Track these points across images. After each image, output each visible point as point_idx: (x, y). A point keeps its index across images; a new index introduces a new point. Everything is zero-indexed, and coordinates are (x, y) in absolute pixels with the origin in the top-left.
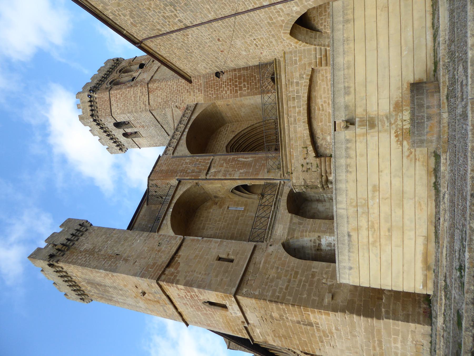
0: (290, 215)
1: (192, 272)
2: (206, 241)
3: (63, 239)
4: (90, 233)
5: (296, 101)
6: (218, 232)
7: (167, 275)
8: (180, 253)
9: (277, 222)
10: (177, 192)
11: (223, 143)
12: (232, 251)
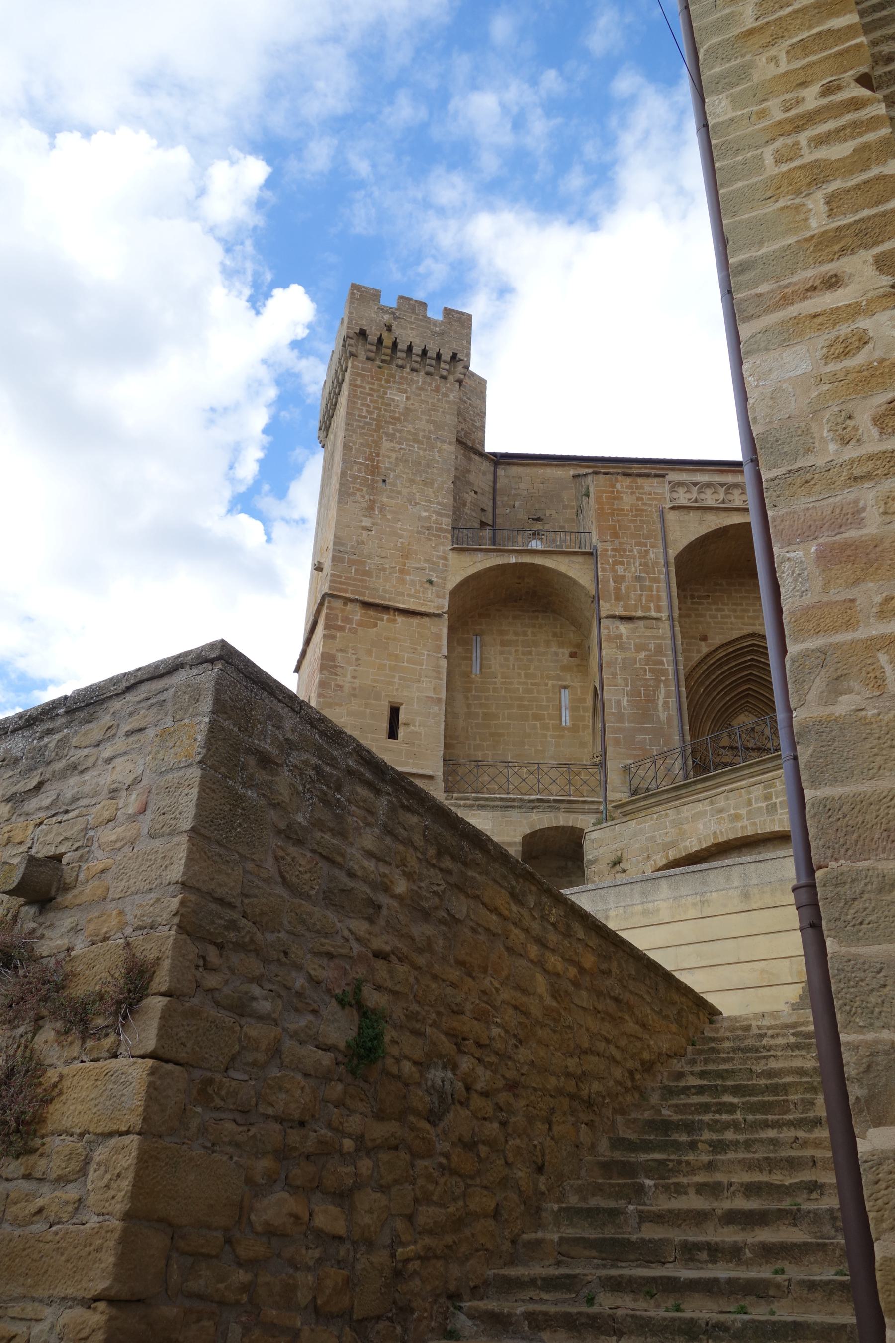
0: (519, 839)
1: (357, 659)
2: (438, 666)
3: (407, 335)
4: (437, 390)
5: (764, 805)
6: (499, 680)
7: (342, 611)
9: (498, 813)
10: (560, 558)
12: (416, 729)
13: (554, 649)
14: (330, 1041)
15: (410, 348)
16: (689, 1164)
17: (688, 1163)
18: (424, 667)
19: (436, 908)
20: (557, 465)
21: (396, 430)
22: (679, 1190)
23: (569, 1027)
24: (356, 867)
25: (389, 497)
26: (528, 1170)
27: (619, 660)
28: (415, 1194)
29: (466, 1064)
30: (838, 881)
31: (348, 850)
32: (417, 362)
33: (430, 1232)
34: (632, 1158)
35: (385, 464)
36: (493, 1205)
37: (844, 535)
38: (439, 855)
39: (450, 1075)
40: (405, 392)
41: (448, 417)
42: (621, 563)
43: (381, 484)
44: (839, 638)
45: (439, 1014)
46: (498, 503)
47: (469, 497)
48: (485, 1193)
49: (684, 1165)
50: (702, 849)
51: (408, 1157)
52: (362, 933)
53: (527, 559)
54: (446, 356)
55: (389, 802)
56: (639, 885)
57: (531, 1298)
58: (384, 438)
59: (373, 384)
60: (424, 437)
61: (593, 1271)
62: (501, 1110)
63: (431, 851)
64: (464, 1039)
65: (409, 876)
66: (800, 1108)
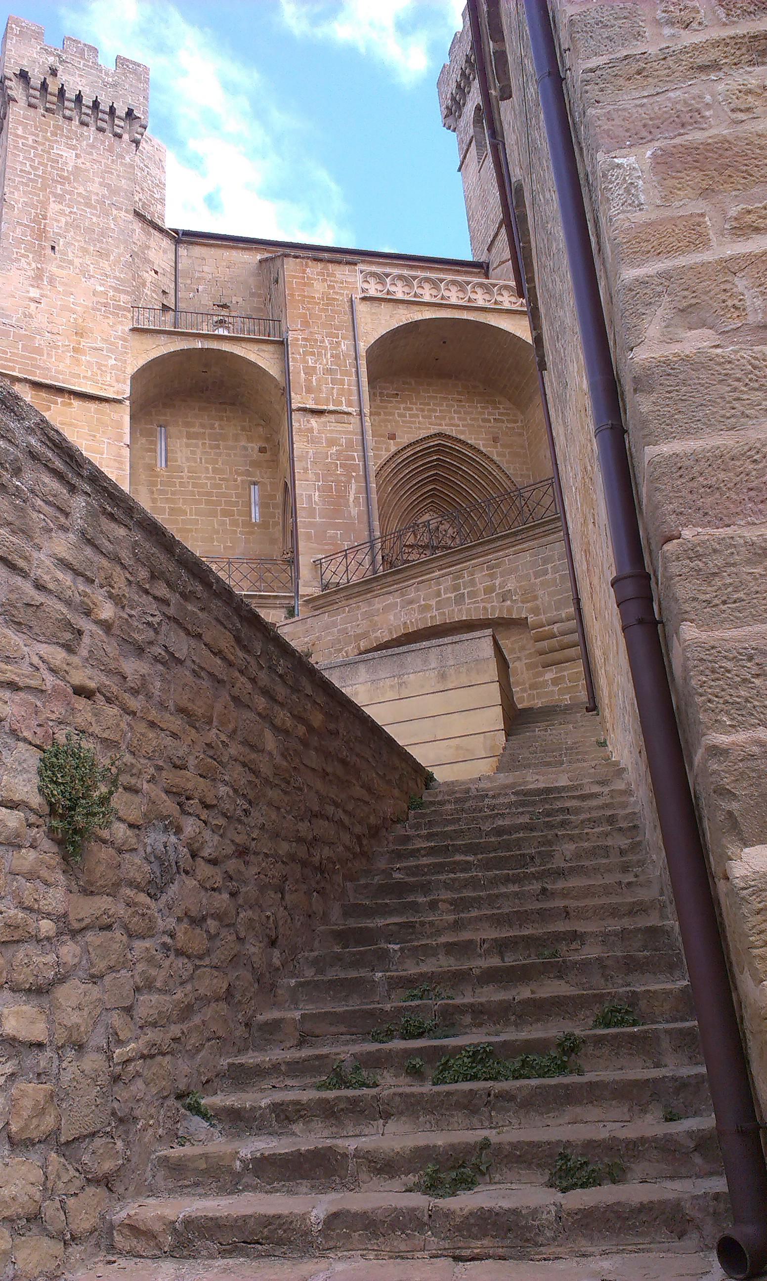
4: (110, 150)
5: (453, 595)
6: (185, 474)
8: (76, 403)
10: (250, 346)
11: (457, 421)
13: (243, 443)
14: (16, 798)
15: (79, 98)
16: (434, 924)
17: (431, 924)
18: (104, 456)
19: (151, 643)
20: (243, 249)
21: (66, 191)
22: (429, 951)
23: (300, 789)
24: (46, 578)
25: (59, 267)
26: (262, 945)
27: (311, 454)
28: (135, 982)
29: (190, 826)
30: (694, 553)
31: (35, 554)
32: (88, 115)
33: (154, 1025)
34: (370, 924)
35: (54, 228)
36: (225, 986)
37: (686, 137)
38: (153, 577)
39: (173, 839)
40: (74, 148)
41: (123, 181)
42: (313, 354)
43: (49, 251)
44: (682, 261)
45: (159, 769)
46: (181, 286)
47: (149, 276)
48: (216, 974)
49: (427, 925)
50: (393, 640)
51: (125, 938)
52: (58, 663)
53: (214, 345)
54: (121, 112)
55: (88, 503)
56: (337, 670)
57: (274, 1087)
58: (52, 199)
59: (38, 136)
60: (98, 201)
61: (345, 1049)
62: (231, 878)
63: (143, 574)
64: (188, 799)
65: (117, 600)
66: (538, 861)
